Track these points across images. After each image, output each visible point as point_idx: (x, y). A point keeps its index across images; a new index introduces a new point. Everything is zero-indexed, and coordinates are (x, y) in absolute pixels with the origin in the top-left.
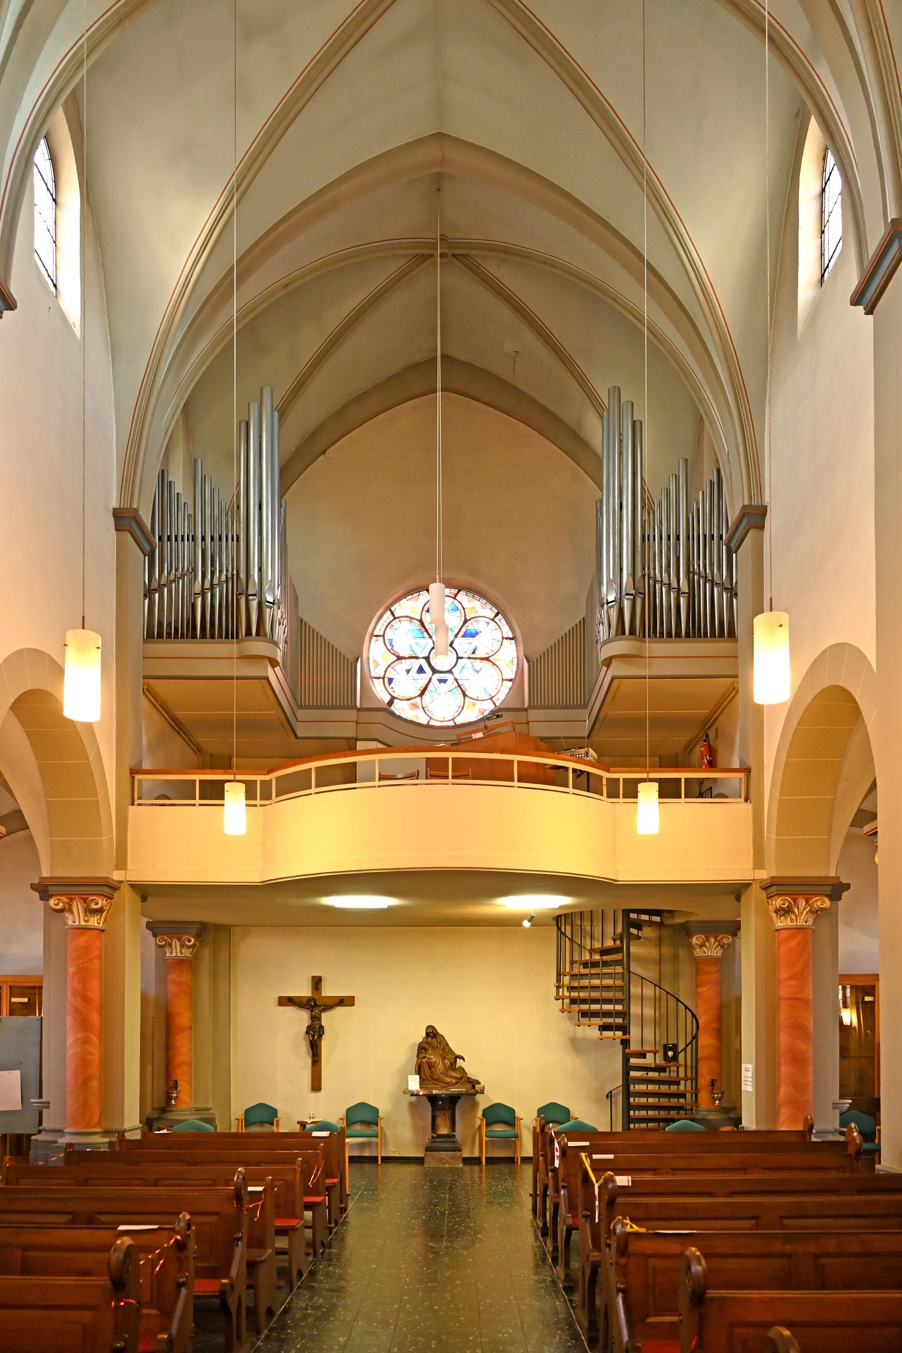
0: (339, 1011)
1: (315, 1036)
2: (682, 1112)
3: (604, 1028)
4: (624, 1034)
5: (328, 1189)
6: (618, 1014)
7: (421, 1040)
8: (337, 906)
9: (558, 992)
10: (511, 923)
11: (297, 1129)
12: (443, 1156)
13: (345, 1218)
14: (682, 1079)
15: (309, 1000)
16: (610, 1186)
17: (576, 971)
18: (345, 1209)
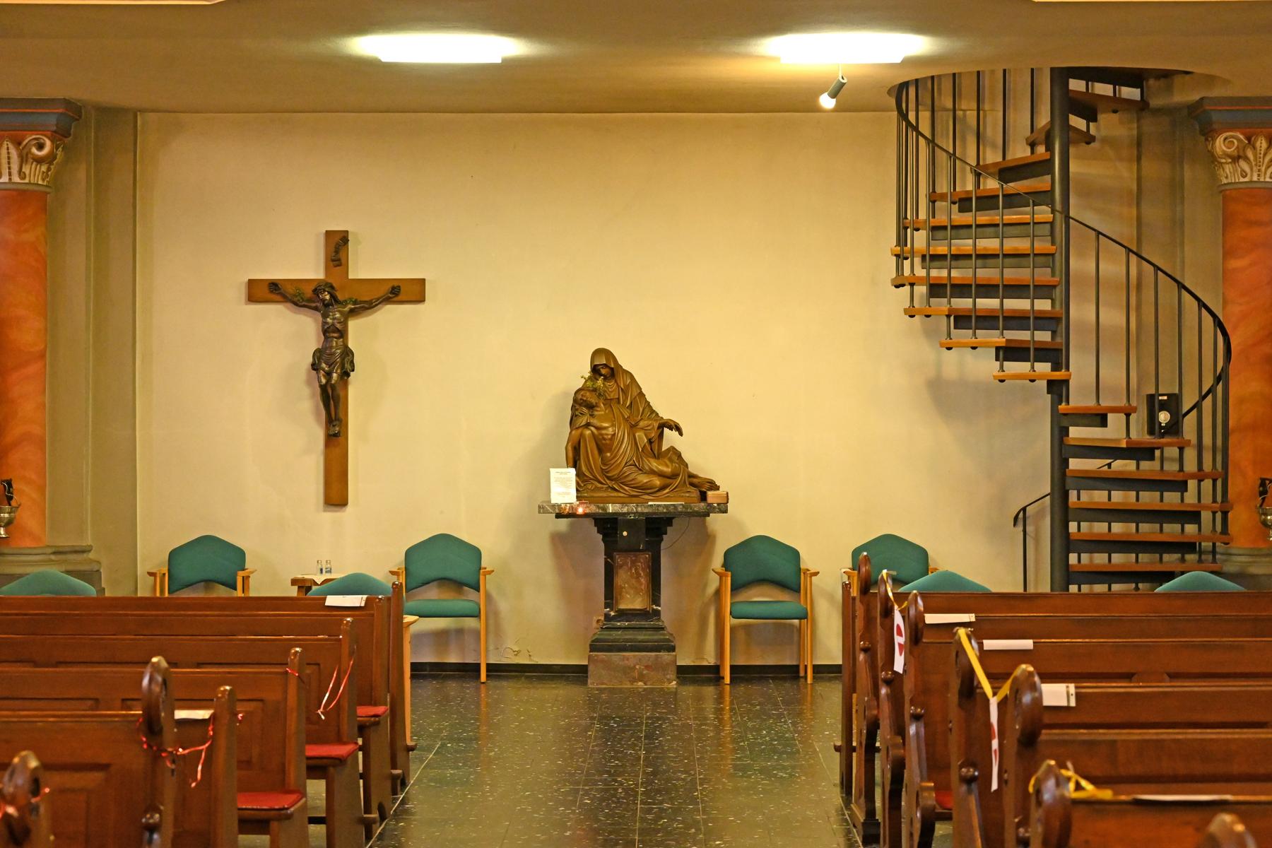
0: (389, 314)
1: (332, 376)
2: (1191, 557)
3: (1009, 353)
4: (1056, 367)
5: (362, 729)
6: (1042, 321)
7: (580, 383)
8: (386, 58)
9: (899, 268)
10: (786, 103)
11: (293, 592)
12: (631, 663)
13: (403, 802)
14: (1192, 476)
15: (319, 288)
16: (1027, 698)
17: (941, 219)
18: (399, 783)
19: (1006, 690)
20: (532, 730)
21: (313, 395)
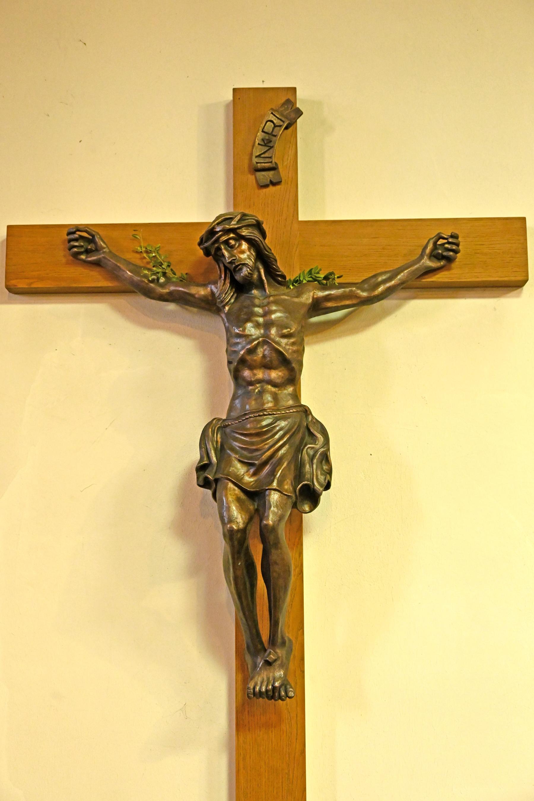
0: (420, 326)
1: (257, 502)
15: (212, 240)
21: (196, 567)
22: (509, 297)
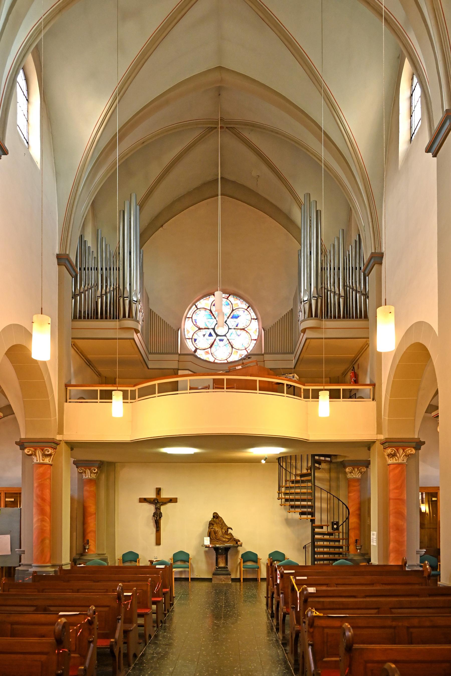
0: (170, 505)
1: (157, 518)
2: (341, 556)
3: (302, 513)
4: (312, 517)
5: (164, 594)
6: (309, 507)
7: (211, 520)
8: (169, 453)
9: (279, 496)
10: (255, 461)
11: (149, 564)
12: (221, 578)
13: (173, 608)
14: (341, 539)
15: (155, 500)
16: (305, 592)
17: (288, 485)
18: (172, 604)
19: (301, 590)
20: (200, 595)
22: (31, 349)
